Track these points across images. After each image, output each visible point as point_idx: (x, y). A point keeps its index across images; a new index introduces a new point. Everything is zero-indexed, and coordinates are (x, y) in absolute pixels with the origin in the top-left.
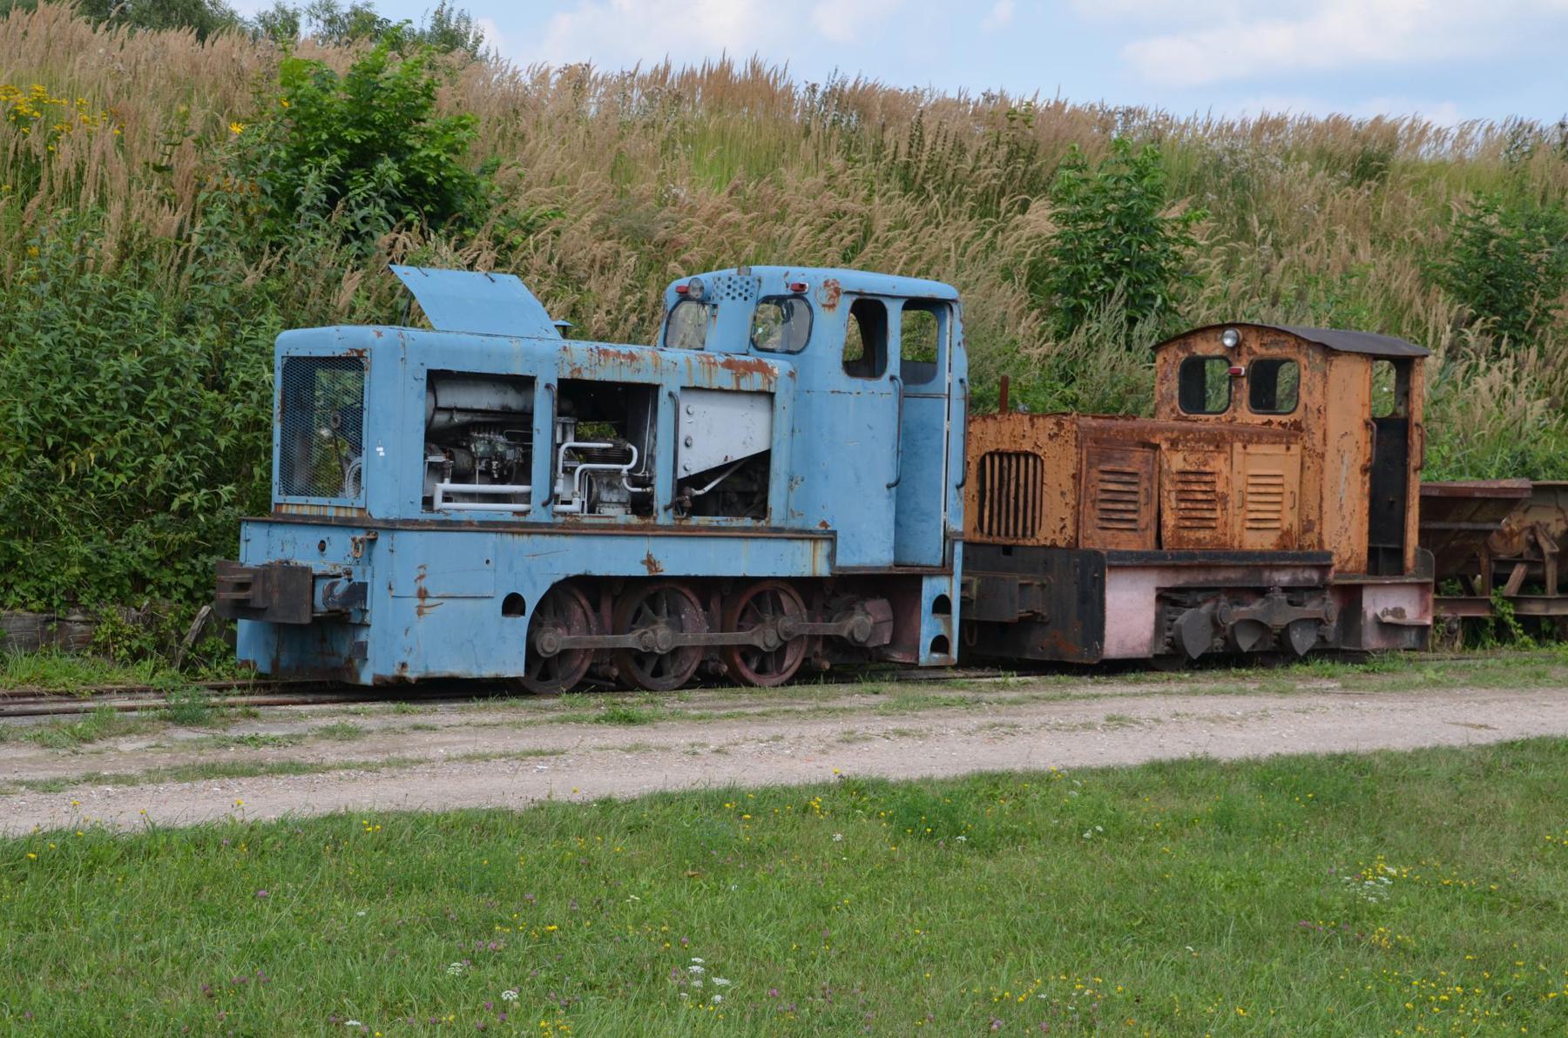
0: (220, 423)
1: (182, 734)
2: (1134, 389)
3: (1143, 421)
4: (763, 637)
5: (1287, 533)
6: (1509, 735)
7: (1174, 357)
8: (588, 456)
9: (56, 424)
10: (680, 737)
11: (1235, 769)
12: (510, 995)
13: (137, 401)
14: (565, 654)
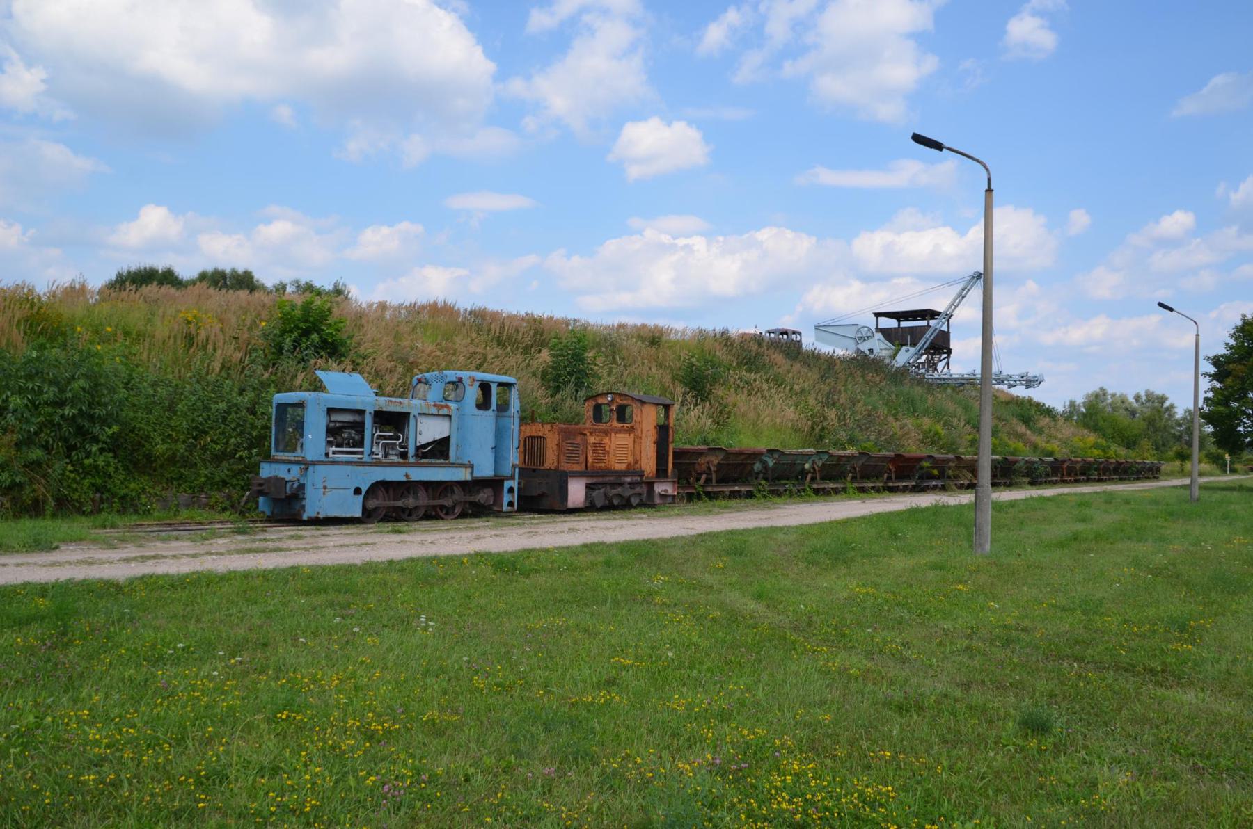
0: (253, 427)
1: (240, 537)
2: (578, 414)
3: (581, 425)
4: (448, 502)
5: (629, 465)
6: (700, 531)
7: (592, 403)
8: (385, 438)
9: (196, 428)
10: (418, 538)
11: (612, 545)
12: (356, 630)
13: (224, 419)
14: (376, 509)
